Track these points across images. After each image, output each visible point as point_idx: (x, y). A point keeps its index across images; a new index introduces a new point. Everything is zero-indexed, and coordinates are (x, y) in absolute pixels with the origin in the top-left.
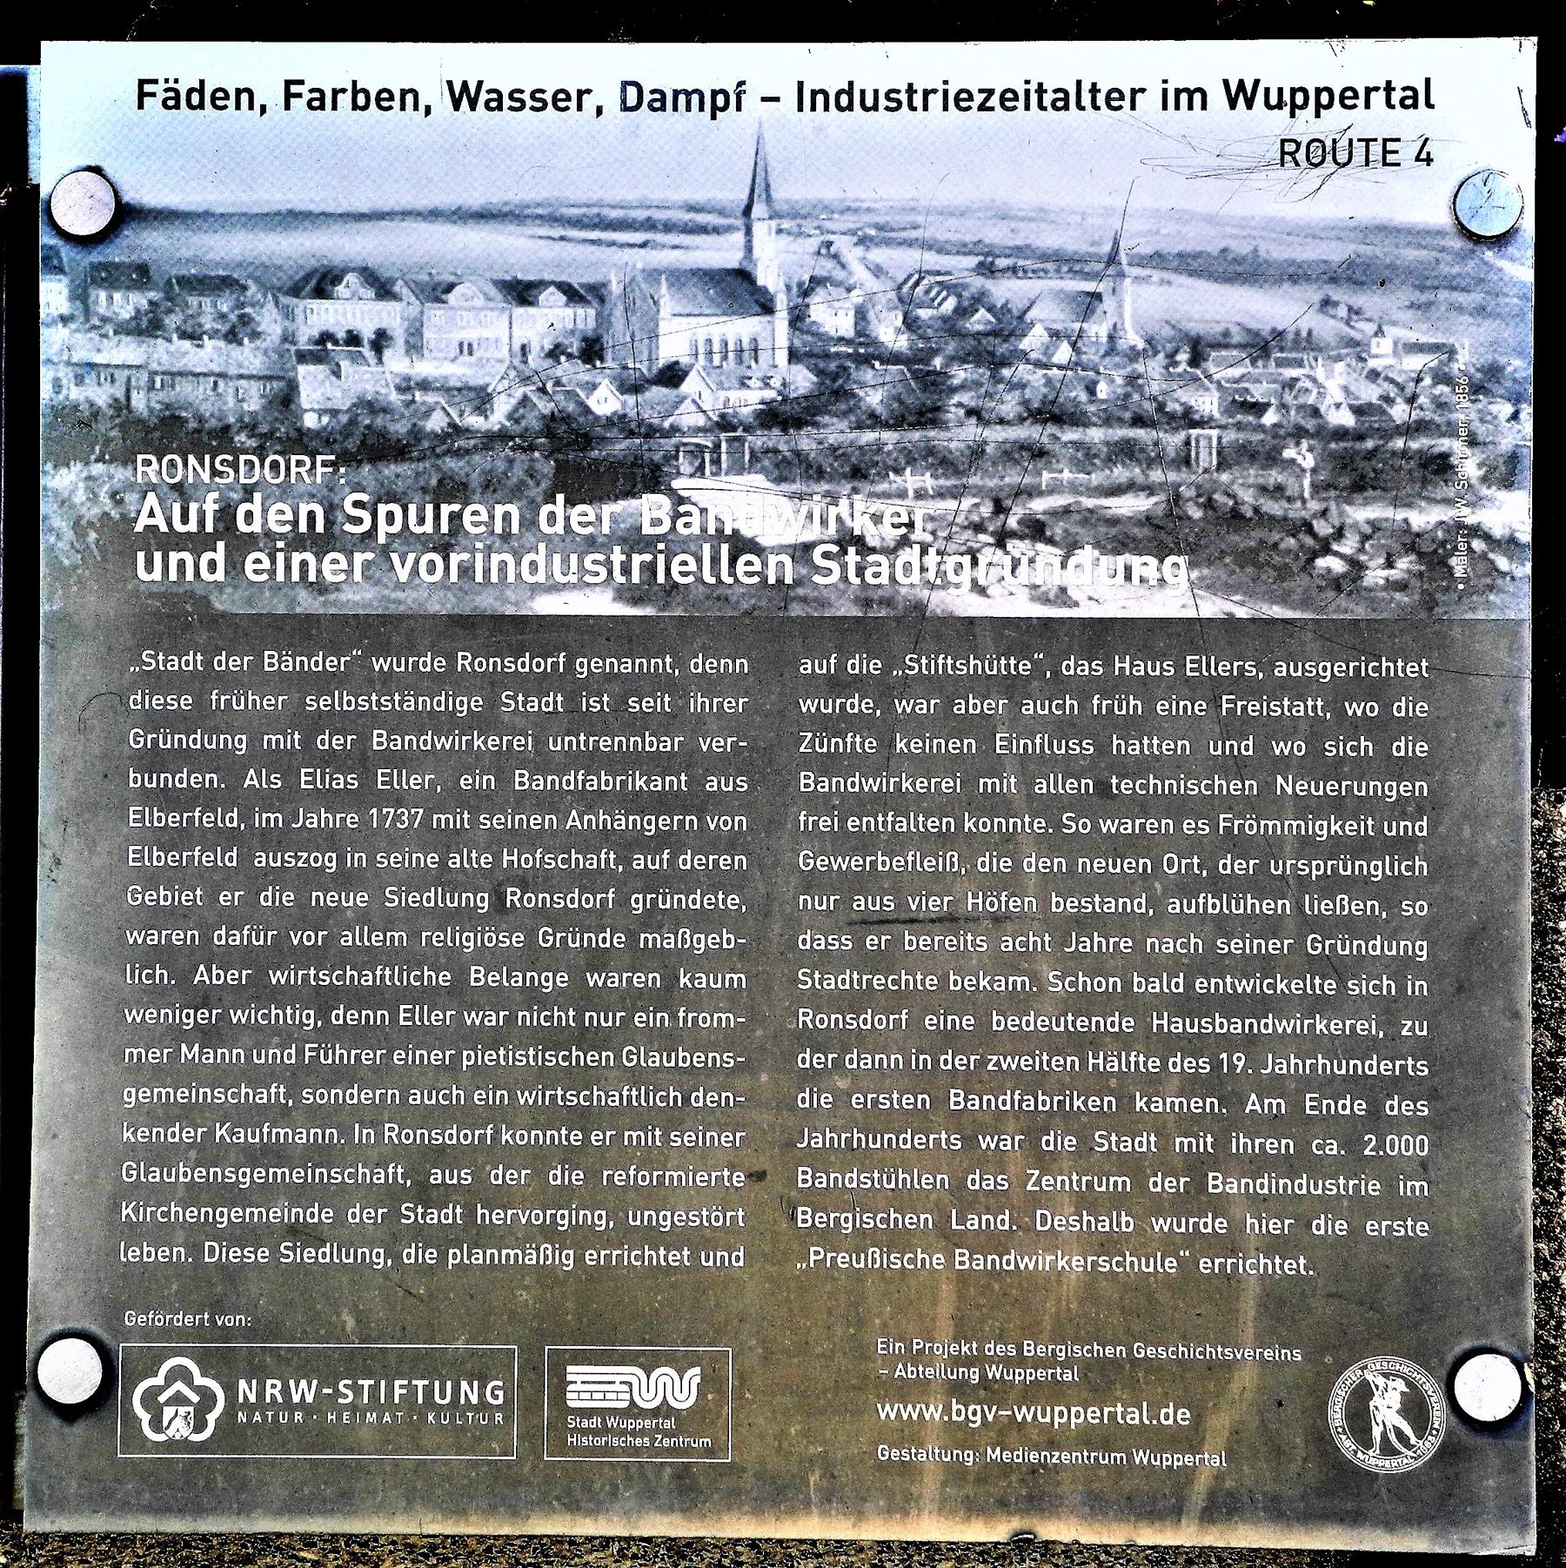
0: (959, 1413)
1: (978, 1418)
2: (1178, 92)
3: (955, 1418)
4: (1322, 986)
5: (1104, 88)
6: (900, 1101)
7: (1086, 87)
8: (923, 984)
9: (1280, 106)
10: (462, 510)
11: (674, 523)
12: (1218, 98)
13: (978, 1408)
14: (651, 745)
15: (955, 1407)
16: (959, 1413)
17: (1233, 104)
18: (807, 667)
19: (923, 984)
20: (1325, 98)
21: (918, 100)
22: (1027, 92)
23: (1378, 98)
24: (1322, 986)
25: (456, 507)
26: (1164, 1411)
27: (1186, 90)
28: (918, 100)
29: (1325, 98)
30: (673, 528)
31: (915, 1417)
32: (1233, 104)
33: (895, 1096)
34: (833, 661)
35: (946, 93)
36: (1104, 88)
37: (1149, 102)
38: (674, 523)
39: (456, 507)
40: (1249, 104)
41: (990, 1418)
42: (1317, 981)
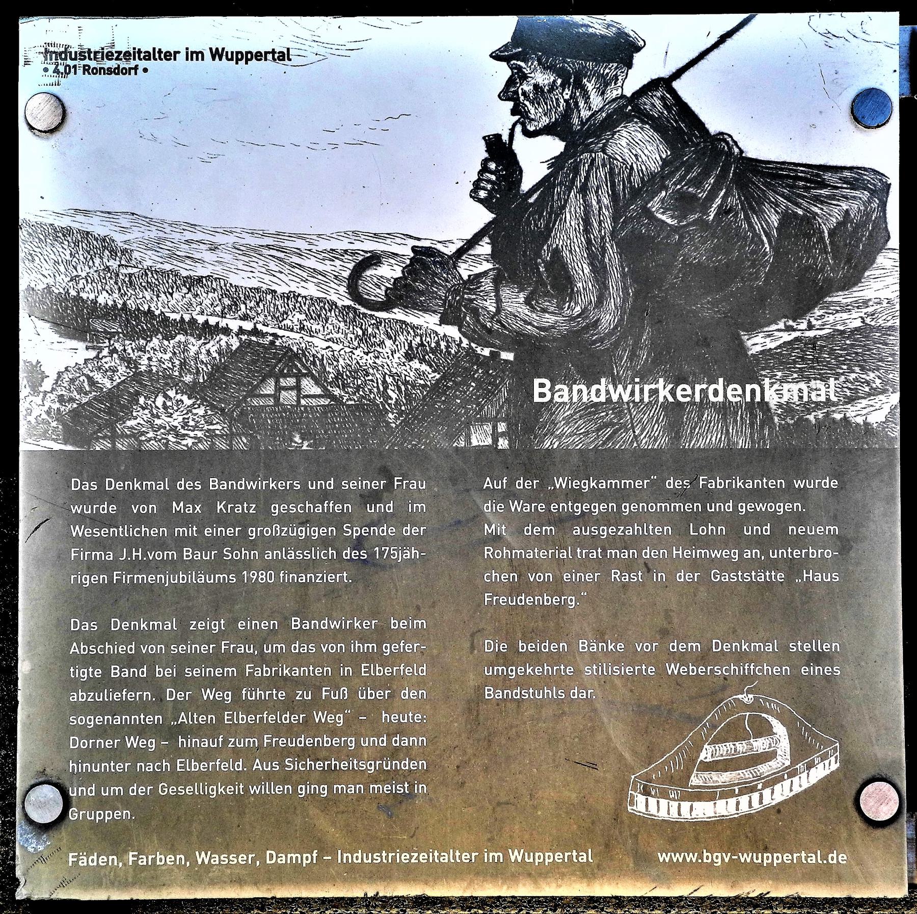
0: (707, 858)
1: (719, 860)
2: (192, 53)
3: (705, 861)
4: (460, 857)
5: (164, 50)
6: (802, 647)
7: (157, 50)
8: (413, 719)
9: (232, 59)
10: (707, 388)
11: (553, 395)
12: (208, 55)
13: (719, 855)
14: (720, 485)
15: (705, 854)
16: (707, 858)
17: (214, 59)
18: (488, 483)
19: (413, 719)
20: (249, 56)
21: (92, 56)
22: (134, 53)
23: (270, 56)
24: (460, 857)
25: (704, 386)
26: (830, 856)
27: (195, 52)
28: (92, 56)
29: (249, 56)
30: (552, 398)
31: (681, 860)
32: (214, 59)
33: (799, 644)
34: (505, 481)
35: (103, 53)
36: (164, 50)
37: (181, 57)
38: (553, 395)
39: (704, 386)
40: (220, 59)
41: (727, 860)
42: (458, 854)
